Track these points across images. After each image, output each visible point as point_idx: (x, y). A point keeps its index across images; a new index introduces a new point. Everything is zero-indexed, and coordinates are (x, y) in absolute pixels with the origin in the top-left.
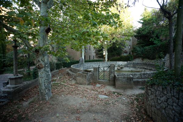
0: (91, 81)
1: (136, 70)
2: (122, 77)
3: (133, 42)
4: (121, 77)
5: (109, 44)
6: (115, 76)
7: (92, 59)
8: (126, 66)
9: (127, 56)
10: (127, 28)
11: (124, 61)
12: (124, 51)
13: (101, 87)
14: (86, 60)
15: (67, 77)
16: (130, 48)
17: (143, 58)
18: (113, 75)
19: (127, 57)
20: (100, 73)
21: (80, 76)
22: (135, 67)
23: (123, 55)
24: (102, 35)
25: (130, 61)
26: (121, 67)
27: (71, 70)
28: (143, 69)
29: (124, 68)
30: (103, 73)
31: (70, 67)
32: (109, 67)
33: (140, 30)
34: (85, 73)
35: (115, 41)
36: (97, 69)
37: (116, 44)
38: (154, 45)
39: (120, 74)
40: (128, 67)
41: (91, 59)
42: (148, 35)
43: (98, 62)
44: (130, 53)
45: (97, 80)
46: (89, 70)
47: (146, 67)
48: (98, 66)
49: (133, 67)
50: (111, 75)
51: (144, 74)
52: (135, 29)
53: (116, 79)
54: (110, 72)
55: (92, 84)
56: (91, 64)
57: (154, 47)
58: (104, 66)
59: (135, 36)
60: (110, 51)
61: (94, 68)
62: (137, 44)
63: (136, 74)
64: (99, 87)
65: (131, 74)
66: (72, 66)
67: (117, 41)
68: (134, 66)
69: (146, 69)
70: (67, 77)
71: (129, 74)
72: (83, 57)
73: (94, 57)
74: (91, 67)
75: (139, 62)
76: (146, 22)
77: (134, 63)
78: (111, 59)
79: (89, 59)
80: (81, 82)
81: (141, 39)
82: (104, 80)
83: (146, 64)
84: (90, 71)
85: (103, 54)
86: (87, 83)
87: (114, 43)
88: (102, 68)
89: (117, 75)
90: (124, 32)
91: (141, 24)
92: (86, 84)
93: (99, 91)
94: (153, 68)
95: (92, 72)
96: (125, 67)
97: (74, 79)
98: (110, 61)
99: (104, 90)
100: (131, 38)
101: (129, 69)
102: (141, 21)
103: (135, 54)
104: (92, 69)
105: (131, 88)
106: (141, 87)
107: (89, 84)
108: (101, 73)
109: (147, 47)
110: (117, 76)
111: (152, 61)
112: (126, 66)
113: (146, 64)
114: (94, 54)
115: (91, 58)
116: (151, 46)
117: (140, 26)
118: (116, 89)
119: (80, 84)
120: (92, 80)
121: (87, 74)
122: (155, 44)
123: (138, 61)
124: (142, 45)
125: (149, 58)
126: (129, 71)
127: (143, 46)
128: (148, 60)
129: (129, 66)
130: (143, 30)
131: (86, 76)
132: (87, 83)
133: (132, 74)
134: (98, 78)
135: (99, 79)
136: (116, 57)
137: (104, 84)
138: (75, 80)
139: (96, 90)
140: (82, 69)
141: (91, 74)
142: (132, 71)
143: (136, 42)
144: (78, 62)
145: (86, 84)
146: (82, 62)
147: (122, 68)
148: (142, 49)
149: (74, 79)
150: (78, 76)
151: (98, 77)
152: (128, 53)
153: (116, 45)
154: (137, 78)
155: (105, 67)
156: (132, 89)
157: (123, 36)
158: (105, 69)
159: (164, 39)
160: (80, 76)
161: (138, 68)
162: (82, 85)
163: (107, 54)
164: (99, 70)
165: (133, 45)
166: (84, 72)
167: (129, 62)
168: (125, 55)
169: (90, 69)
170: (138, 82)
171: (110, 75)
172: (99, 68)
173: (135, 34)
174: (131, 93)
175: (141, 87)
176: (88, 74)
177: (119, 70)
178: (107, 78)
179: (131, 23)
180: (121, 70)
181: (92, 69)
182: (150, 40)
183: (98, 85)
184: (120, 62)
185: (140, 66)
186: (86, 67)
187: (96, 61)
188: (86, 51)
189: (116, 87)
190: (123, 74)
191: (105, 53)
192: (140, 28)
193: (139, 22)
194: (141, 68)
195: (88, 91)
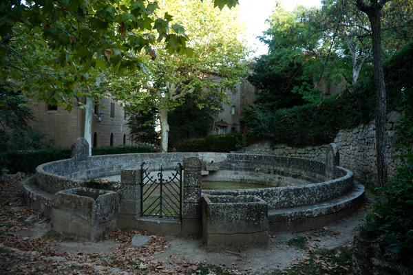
0: (113, 223)
1: (255, 178)
2: (230, 207)
3: (243, 97)
4: (224, 207)
5: (174, 98)
6: (202, 201)
7: (118, 143)
8: (226, 166)
9: (228, 138)
10: (228, 51)
11: (218, 152)
12: (217, 120)
13: (150, 247)
14: (99, 145)
15: (14, 209)
16: (233, 113)
17: (274, 143)
18: (193, 198)
19: (226, 138)
20: (144, 197)
21: (67, 205)
22: (251, 170)
23: (214, 133)
24: (161, 25)
25: (236, 150)
26: (212, 168)
27: (35, 183)
28: (274, 173)
29: (218, 173)
30: (158, 190)
31: (34, 171)
32: (181, 168)
33: (263, 62)
34: (87, 194)
35: (191, 91)
36: (134, 176)
37: (195, 98)
38: (304, 106)
39: (219, 194)
40: (230, 169)
41: (116, 145)
42: (287, 76)
43: (139, 154)
44: (233, 129)
45: (137, 221)
46: (105, 180)
47: (282, 169)
48: (138, 168)
49: (246, 170)
50: (189, 199)
51: (298, 190)
52: (250, 58)
53: (207, 212)
54: (185, 189)
55: (116, 236)
56: (115, 161)
57: (305, 110)
58: (161, 168)
59: (250, 79)
60: (174, 119)
61: (124, 174)
62: (255, 103)
63: (273, 194)
64: (143, 249)
65: (258, 194)
66: (40, 169)
67: (198, 89)
68: (250, 165)
69: (283, 173)
70: (14, 209)
71: (249, 193)
72: (88, 138)
73: (127, 138)
74: (115, 170)
75: (263, 154)
76: (282, 39)
77: (248, 156)
78: (180, 143)
79: (109, 144)
80: (70, 229)
81: (265, 87)
82: (161, 217)
83: (281, 160)
84: (108, 186)
85: (153, 129)
86: (95, 231)
87: (187, 96)
88: (155, 175)
89: (212, 199)
90: (218, 64)
91: (267, 45)
92: (89, 238)
93: (142, 266)
94: (303, 172)
95: (114, 189)
96: (222, 168)
97: (42, 216)
98: (177, 151)
99: (164, 259)
100: (238, 83)
101: (235, 177)
102: (266, 35)
103: (251, 131)
104: (117, 179)
105: (263, 244)
106: (290, 237)
107: (101, 238)
108: (149, 192)
109: (284, 111)
110: (209, 202)
111: (300, 151)
112: (226, 166)
113: (284, 160)
114: (127, 131)
115: (115, 141)
116: (295, 107)
117: (264, 50)
118: (209, 251)
119: (65, 240)
120: (114, 221)
121: (95, 196)
122: (307, 102)
123: (259, 150)
124: (270, 104)
125: (290, 143)
126: (234, 182)
127: (272, 109)
128: (287, 148)
129: (234, 165)
130: (272, 62)
131: (90, 206)
132: (95, 231)
133: (262, 192)
134: (138, 211)
135: (142, 215)
136: (195, 139)
137: (160, 234)
138: (48, 220)
139: (131, 263)
140: (80, 177)
141: (112, 198)
142: (242, 183)
143: (252, 98)
144: (67, 154)
145: (89, 238)
146: (83, 153)
147: (212, 172)
148: (270, 115)
149: (42, 216)
150: (57, 208)
151: (138, 207)
152: (229, 128)
153: (196, 101)
154: (279, 206)
155: (167, 169)
156: (265, 249)
157: (216, 77)
158: (167, 175)
159: (324, 92)
160: (67, 205)
161: (261, 170)
162: (72, 240)
163: (166, 128)
164: (142, 180)
165: (242, 105)
166: (84, 189)
167: (232, 153)
168: (221, 132)
169: (111, 175)
170: (281, 219)
171: (185, 198)
172: (142, 171)
173: (251, 72)
174: (263, 264)
175: (290, 237)
176: (101, 198)
177: (205, 179)
178: (172, 208)
179: (240, 39)
180: (209, 179)
181: (117, 179)
182: (294, 91)
183: (139, 240)
184: (209, 153)
185: (265, 164)
186: (95, 172)
187: (133, 150)
188: (100, 119)
189: (209, 242)
190: (229, 194)
191: (160, 127)
192: (263, 56)
193: (261, 39)
194: (269, 173)
195: (96, 268)
